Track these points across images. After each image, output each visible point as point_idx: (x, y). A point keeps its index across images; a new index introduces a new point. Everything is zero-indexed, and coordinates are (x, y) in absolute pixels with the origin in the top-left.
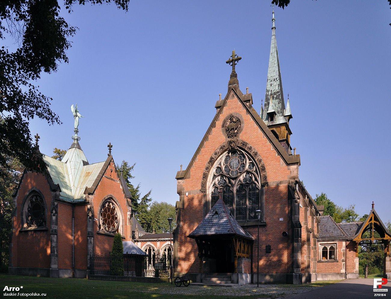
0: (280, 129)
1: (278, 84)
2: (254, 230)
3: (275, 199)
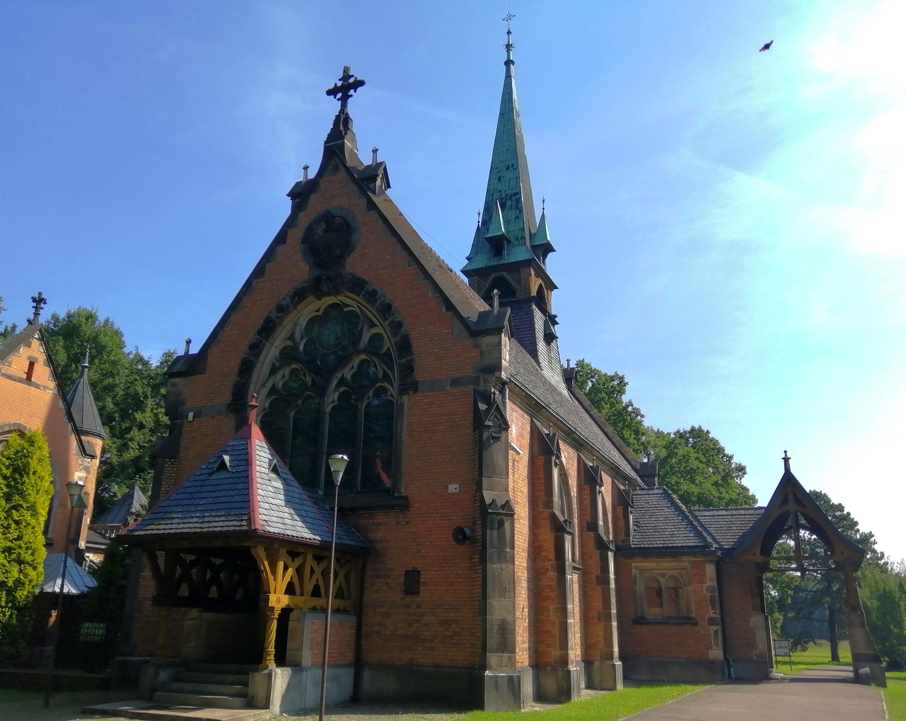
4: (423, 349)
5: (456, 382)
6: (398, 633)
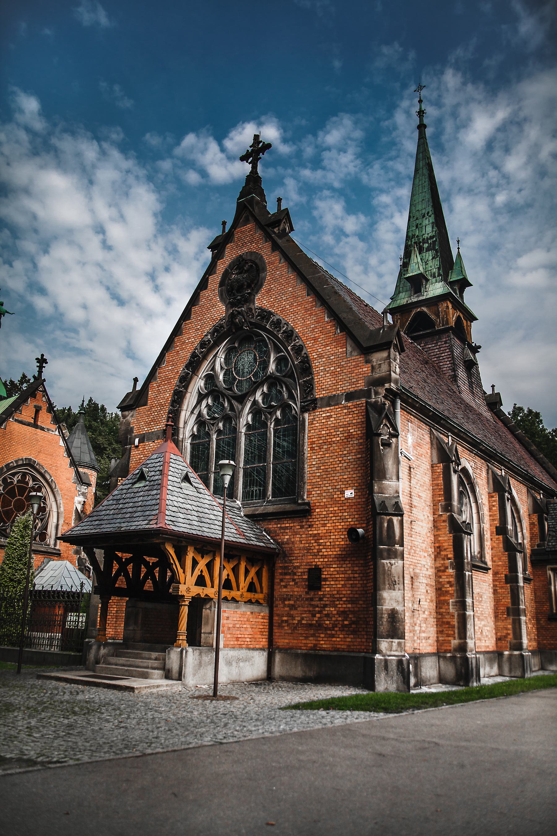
0: (436, 309)
1: (431, 222)
2: (279, 526)
3: (334, 439)
4: (321, 368)
5: (350, 397)
6: (304, 622)
